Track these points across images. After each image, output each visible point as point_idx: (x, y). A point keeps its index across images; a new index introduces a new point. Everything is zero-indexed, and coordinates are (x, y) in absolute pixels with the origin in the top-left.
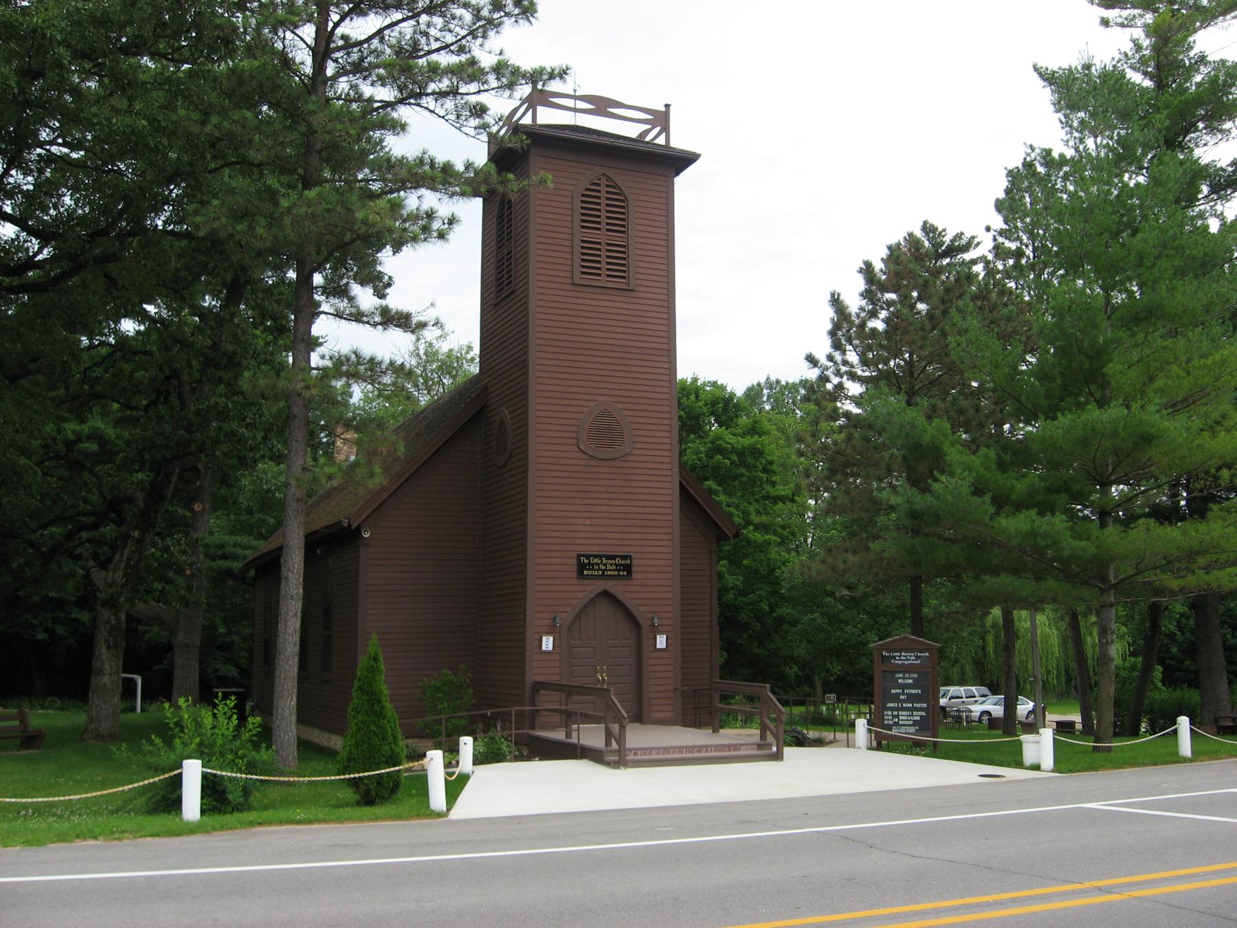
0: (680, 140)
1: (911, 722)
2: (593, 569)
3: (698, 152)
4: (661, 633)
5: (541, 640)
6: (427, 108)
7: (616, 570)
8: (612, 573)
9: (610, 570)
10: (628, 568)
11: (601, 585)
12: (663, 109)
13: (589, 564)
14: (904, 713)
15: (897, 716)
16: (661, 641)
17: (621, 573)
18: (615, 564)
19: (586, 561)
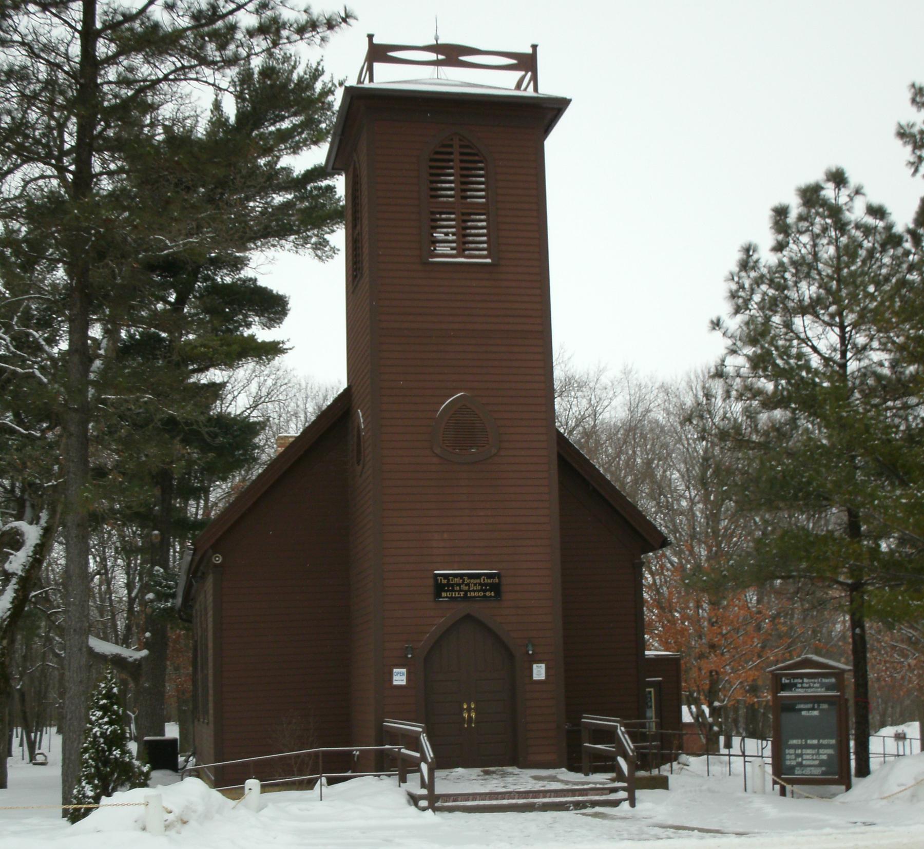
0: (549, 87)
1: (817, 762)
2: (453, 590)
3: (568, 97)
4: (539, 661)
5: (409, 679)
6: (206, 82)
7: (481, 590)
8: (476, 594)
9: (474, 591)
10: (496, 588)
11: (463, 608)
12: (530, 51)
13: (448, 585)
14: (809, 751)
15: (801, 755)
16: (539, 672)
17: (488, 594)
18: (480, 584)
19: (445, 582)
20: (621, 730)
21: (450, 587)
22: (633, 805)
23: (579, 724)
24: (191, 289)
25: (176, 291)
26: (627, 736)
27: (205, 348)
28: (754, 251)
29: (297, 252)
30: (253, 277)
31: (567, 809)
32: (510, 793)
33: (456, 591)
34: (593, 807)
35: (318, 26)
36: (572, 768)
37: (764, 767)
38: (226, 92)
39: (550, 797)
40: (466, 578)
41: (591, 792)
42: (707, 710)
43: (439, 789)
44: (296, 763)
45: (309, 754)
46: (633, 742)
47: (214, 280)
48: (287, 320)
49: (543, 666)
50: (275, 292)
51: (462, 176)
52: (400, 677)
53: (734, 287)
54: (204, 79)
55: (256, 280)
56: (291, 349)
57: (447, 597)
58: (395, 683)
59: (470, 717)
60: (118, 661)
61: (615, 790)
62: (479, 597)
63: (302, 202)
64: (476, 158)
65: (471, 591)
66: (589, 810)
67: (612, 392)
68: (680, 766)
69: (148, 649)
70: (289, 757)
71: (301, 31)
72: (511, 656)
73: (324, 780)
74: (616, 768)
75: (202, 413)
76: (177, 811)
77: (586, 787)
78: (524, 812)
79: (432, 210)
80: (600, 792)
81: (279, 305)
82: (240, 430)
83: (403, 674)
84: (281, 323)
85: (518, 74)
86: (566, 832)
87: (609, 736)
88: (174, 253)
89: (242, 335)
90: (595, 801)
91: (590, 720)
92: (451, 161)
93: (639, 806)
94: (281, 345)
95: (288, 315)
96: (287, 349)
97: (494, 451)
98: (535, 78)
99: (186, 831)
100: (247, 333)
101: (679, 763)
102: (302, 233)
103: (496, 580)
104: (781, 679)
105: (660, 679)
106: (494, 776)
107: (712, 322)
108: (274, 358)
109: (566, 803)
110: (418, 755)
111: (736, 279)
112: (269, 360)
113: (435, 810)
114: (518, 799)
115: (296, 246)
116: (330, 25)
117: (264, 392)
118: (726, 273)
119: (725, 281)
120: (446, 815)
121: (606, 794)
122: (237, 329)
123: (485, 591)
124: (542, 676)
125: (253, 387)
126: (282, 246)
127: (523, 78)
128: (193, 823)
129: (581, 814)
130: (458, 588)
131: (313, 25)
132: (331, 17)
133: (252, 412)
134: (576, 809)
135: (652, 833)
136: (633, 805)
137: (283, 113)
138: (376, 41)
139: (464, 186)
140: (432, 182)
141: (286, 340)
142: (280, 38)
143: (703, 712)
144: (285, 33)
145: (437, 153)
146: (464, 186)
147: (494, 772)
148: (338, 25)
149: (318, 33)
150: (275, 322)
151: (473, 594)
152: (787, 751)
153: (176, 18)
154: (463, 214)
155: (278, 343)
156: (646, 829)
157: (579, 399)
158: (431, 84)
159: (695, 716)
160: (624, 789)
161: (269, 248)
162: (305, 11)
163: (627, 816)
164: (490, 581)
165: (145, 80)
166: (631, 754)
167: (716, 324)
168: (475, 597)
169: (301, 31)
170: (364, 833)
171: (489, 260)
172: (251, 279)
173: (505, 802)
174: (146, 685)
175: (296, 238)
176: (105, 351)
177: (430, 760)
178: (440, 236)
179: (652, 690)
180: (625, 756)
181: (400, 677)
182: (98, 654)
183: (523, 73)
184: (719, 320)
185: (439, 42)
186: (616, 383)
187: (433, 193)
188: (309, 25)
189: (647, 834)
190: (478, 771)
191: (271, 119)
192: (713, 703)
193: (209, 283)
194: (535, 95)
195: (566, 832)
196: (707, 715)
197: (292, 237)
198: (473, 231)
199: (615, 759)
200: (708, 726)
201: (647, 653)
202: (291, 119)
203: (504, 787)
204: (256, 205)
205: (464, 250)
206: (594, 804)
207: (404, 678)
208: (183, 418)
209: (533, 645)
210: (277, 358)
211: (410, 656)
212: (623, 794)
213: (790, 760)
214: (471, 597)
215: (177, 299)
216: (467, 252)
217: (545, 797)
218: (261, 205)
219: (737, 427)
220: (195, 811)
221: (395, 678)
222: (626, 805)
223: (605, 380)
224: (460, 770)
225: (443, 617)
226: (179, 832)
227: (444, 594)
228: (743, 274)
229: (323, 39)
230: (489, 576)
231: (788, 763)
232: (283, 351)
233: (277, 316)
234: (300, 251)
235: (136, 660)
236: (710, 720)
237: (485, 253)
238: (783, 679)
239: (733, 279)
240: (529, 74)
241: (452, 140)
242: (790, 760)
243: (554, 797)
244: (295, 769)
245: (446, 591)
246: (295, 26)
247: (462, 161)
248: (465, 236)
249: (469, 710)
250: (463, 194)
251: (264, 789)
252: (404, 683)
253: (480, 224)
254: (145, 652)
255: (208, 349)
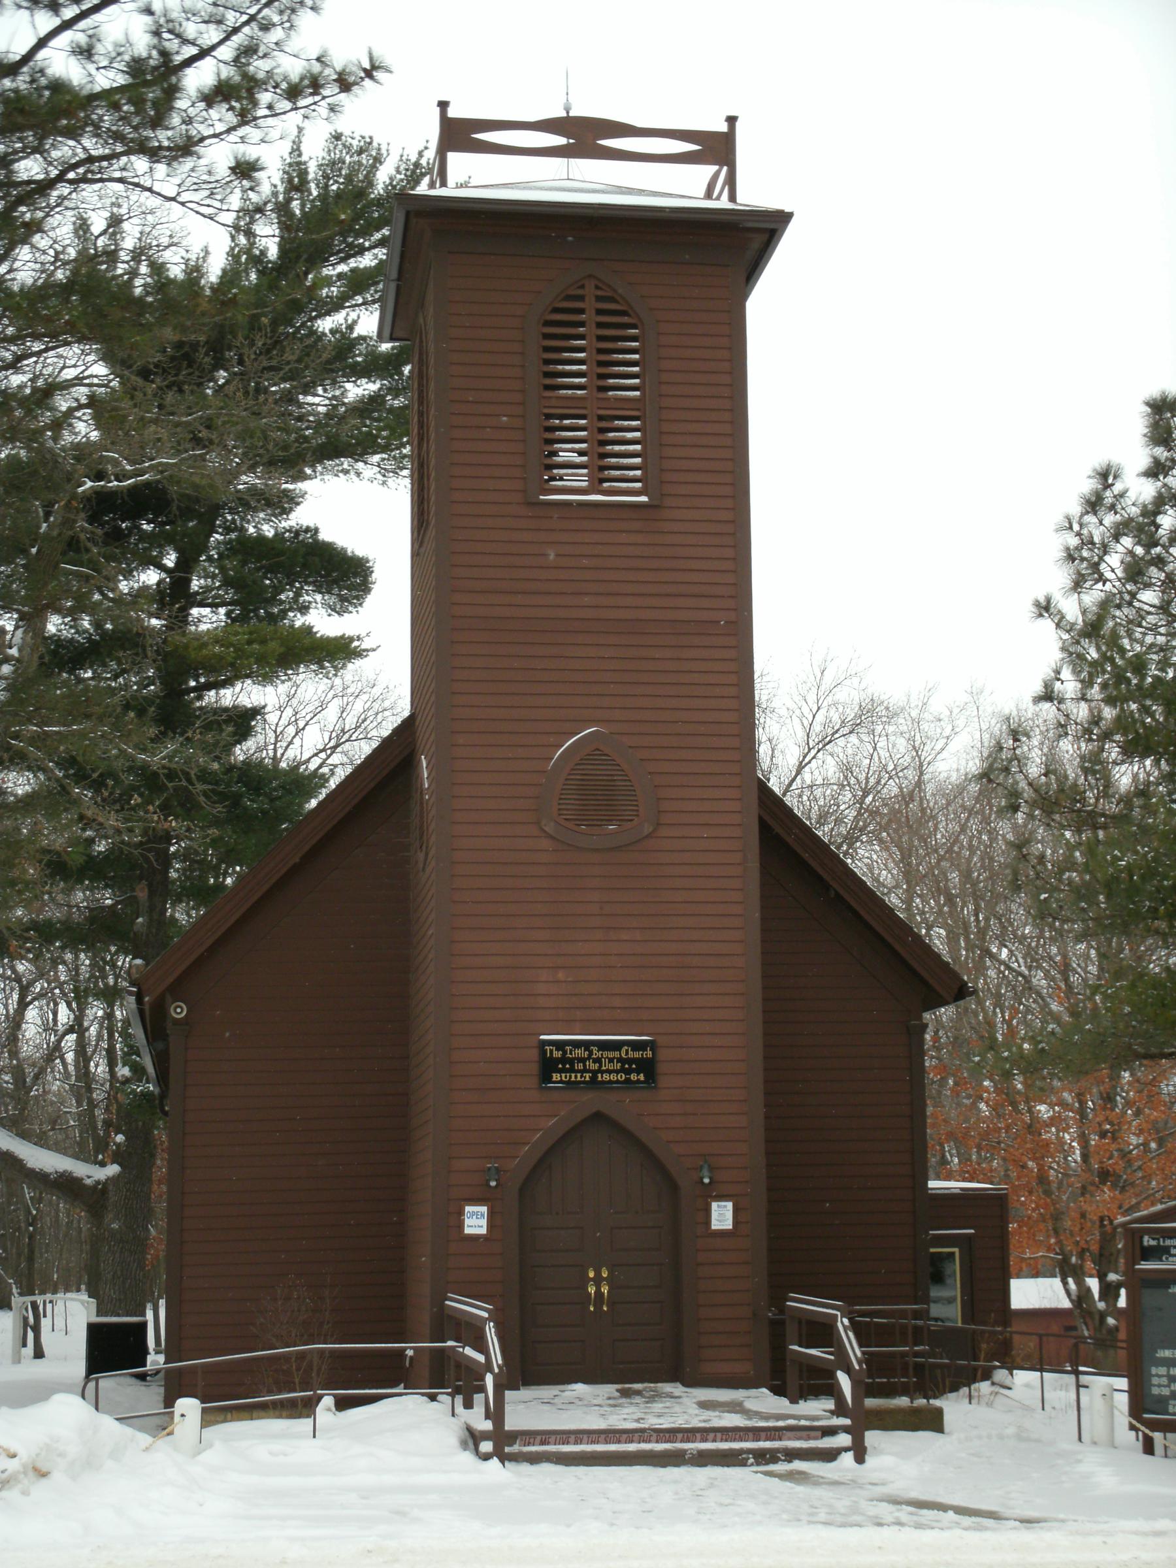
2: (572, 1070)
7: (622, 1070)
8: (613, 1077)
9: (609, 1072)
10: (648, 1067)
11: (590, 1101)
12: (723, 127)
13: (563, 1060)
16: (722, 1216)
17: (633, 1077)
18: (620, 1060)
19: (557, 1054)
20: (842, 1323)
21: (567, 1064)
22: (860, 1459)
23: (782, 1310)
24: (204, 547)
25: (176, 550)
26: (851, 1334)
27: (222, 646)
28: (1115, 477)
29: (384, 483)
30: (312, 525)
31: (743, 1464)
32: (643, 1430)
33: (578, 1071)
34: (790, 1461)
35: (322, 86)
36: (778, 1391)
37: (1112, 1398)
38: (173, 203)
39: (714, 1441)
40: (595, 1049)
41: (789, 1434)
42: (1093, 1284)
43: (511, 1424)
44: (298, 1369)
45: (322, 1351)
46: (861, 1345)
47: (242, 530)
48: (370, 600)
49: (729, 1205)
50: (349, 553)
51: (600, 351)
52: (476, 1221)
53: (1074, 541)
54: (136, 180)
55: (316, 530)
56: (374, 650)
57: (561, 1082)
58: (467, 1231)
59: (599, 1293)
60: (66, 1184)
61: (830, 1431)
62: (617, 1082)
63: (396, 397)
64: (626, 319)
65: (603, 1072)
66: (781, 1467)
67: (950, 727)
68: (996, 1389)
69: (120, 1164)
70: (286, 1357)
71: (293, 93)
72: (674, 1187)
73: (328, 1401)
74: (832, 1390)
75: (217, 758)
76: (24, 1455)
77: (781, 1424)
78: (664, 1466)
79: (546, 411)
80: (804, 1434)
81: (356, 575)
82: (282, 787)
83: (482, 1215)
84: (361, 605)
85: (709, 170)
86: (721, 1505)
87: (822, 1333)
88: (147, 484)
89: (292, 626)
90: (794, 1449)
91: (802, 1304)
92: (582, 324)
93: (870, 1460)
94: (356, 644)
95: (373, 592)
96: (367, 650)
97: (647, 829)
98: (731, 181)
99: (41, 1489)
100: (299, 621)
101: (993, 1384)
102: (392, 450)
103: (649, 1054)
104: (1141, 1238)
105: (973, 1231)
106: (638, 1399)
107: (1037, 604)
108: (344, 666)
109: (741, 1451)
110: (481, 1358)
111: (1076, 527)
112: (336, 669)
113: (504, 1458)
114: (657, 1442)
115: (384, 472)
116: (345, 84)
117: (350, 722)
118: (1059, 518)
119: (1057, 531)
120: (525, 1468)
121: (816, 1438)
122: (284, 613)
123: (628, 1072)
124: (728, 1224)
125: (331, 714)
126: (358, 474)
127: (716, 176)
128: (57, 1477)
129: (762, 1472)
130: (581, 1066)
131: (315, 84)
132: (344, 70)
133: (329, 757)
134: (758, 1464)
135: (870, 1513)
136: (860, 1459)
137: (361, 241)
138: (452, 113)
139: (603, 369)
140: (547, 362)
141: (363, 634)
142: (255, 103)
143: (1089, 1290)
144: (265, 97)
145: (556, 310)
146: (603, 369)
147: (638, 1393)
148: (357, 84)
149: (324, 98)
150: (351, 603)
151: (606, 1077)
152: (1154, 1370)
153: (93, 72)
154: (601, 418)
155: (351, 639)
156: (864, 1504)
157: (892, 738)
158: (541, 189)
159: (1074, 1297)
160: (846, 1429)
161: (336, 475)
162: (318, 59)
163: (842, 1480)
164: (638, 1055)
165: (29, 182)
166: (857, 1367)
167: (1045, 608)
168: (610, 1082)
169: (293, 93)
170: (364, 1498)
171: (644, 499)
172: (308, 530)
173: (632, 1447)
174: (115, 1226)
175: (383, 459)
176: (20, 650)
177: (496, 1370)
178: (565, 456)
179: (956, 1250)
180: (848, 1370)
181: (476, 1221)
182: (32, 1171)
183: (716, 168)
184: (1048, 600)
185: (572, 114)
186: (956, 711)
187: (548, 381)
188: (306, 82)
189: (863, 1514)
190: (610, 1389)
191: (340, 251)
192: (1106, 1275)
193: (233, 536)
194: (730, 206)
195: (721, 1505)
196: (1096, 1296)
197: (376, 458)
198: (617, 448)
199: (832, 1376)
200: (1097, 1317)
201: (932, 1184)
202: (376, 251)
203: (638, 1421)
204: (318, 401)
205: (602, 481)
206: (792, 1455)
207: (484, 1222)
208: (164, 767)
209: (711, 1169)
210: (350, 666)
211: (493, 1184)
212: (844, 1440)
213: (1159, 1386)
214: (603, 1082)
215: (178, 563)
216: (606, 485)
217: (704, 1440)
218: (327, 402)
219: (1075, 794)
220: (62, 1455)
221: (467, 1222)
222: (848, 1458)
223: (937, 706)
224: (580, 1388)
225: (556, 1116)
226: (25, 1493)
227: (556, 1077)
228: (1091, 519)
229: (332, 109)
230: (636, 1046)
231: (1155, 1391)
232: (358, 654)
233: (354, 593)
234: (390, 482)
235: (98, 1182)
236: (1101, 1305)
237: (639, 485)
238: (1146, 1238)
239: (1071, 528)
240: (725, 168)
241: (582, 287)
242: (1159, 1386)
243: (722, 1440)
244: (297, 1380)
245: (560, 1071)
246: (284, 86)
247: (600, 325)
248: (603, 456)
249: (598, 1281)
250: (601, 383)
251: (209, 1418)
252: (483, 1231)
253: (629, 435)
254: (113, 1170)
255: (228, 648)
